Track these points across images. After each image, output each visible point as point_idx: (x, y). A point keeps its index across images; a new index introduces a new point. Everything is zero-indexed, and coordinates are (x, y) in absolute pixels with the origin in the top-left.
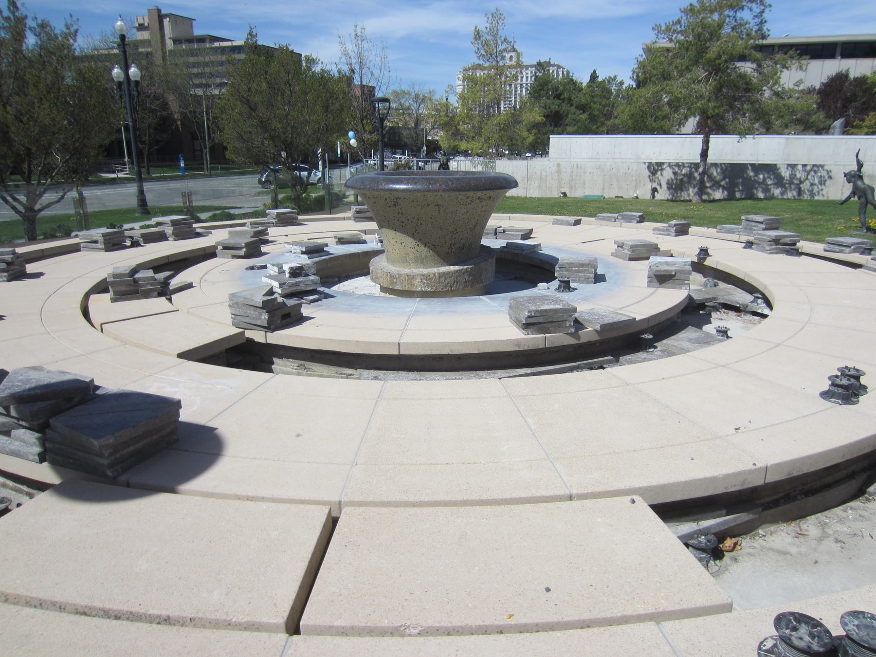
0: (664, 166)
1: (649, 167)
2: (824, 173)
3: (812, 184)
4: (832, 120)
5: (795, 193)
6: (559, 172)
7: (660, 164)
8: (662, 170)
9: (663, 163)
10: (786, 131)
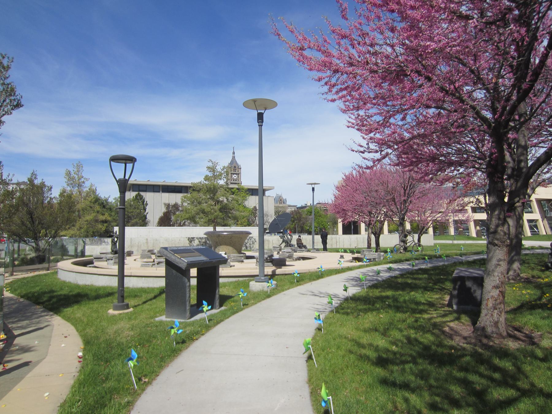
0: (195, 239)
1: (188, 239)
2: (253, 240)
3: (250, 244)
4: (541, 58)
5: (245, 248)
6: (147, 243)
7: (193, 238)
8: (194, 240)
9: (194, 238)
10: (90, 357)
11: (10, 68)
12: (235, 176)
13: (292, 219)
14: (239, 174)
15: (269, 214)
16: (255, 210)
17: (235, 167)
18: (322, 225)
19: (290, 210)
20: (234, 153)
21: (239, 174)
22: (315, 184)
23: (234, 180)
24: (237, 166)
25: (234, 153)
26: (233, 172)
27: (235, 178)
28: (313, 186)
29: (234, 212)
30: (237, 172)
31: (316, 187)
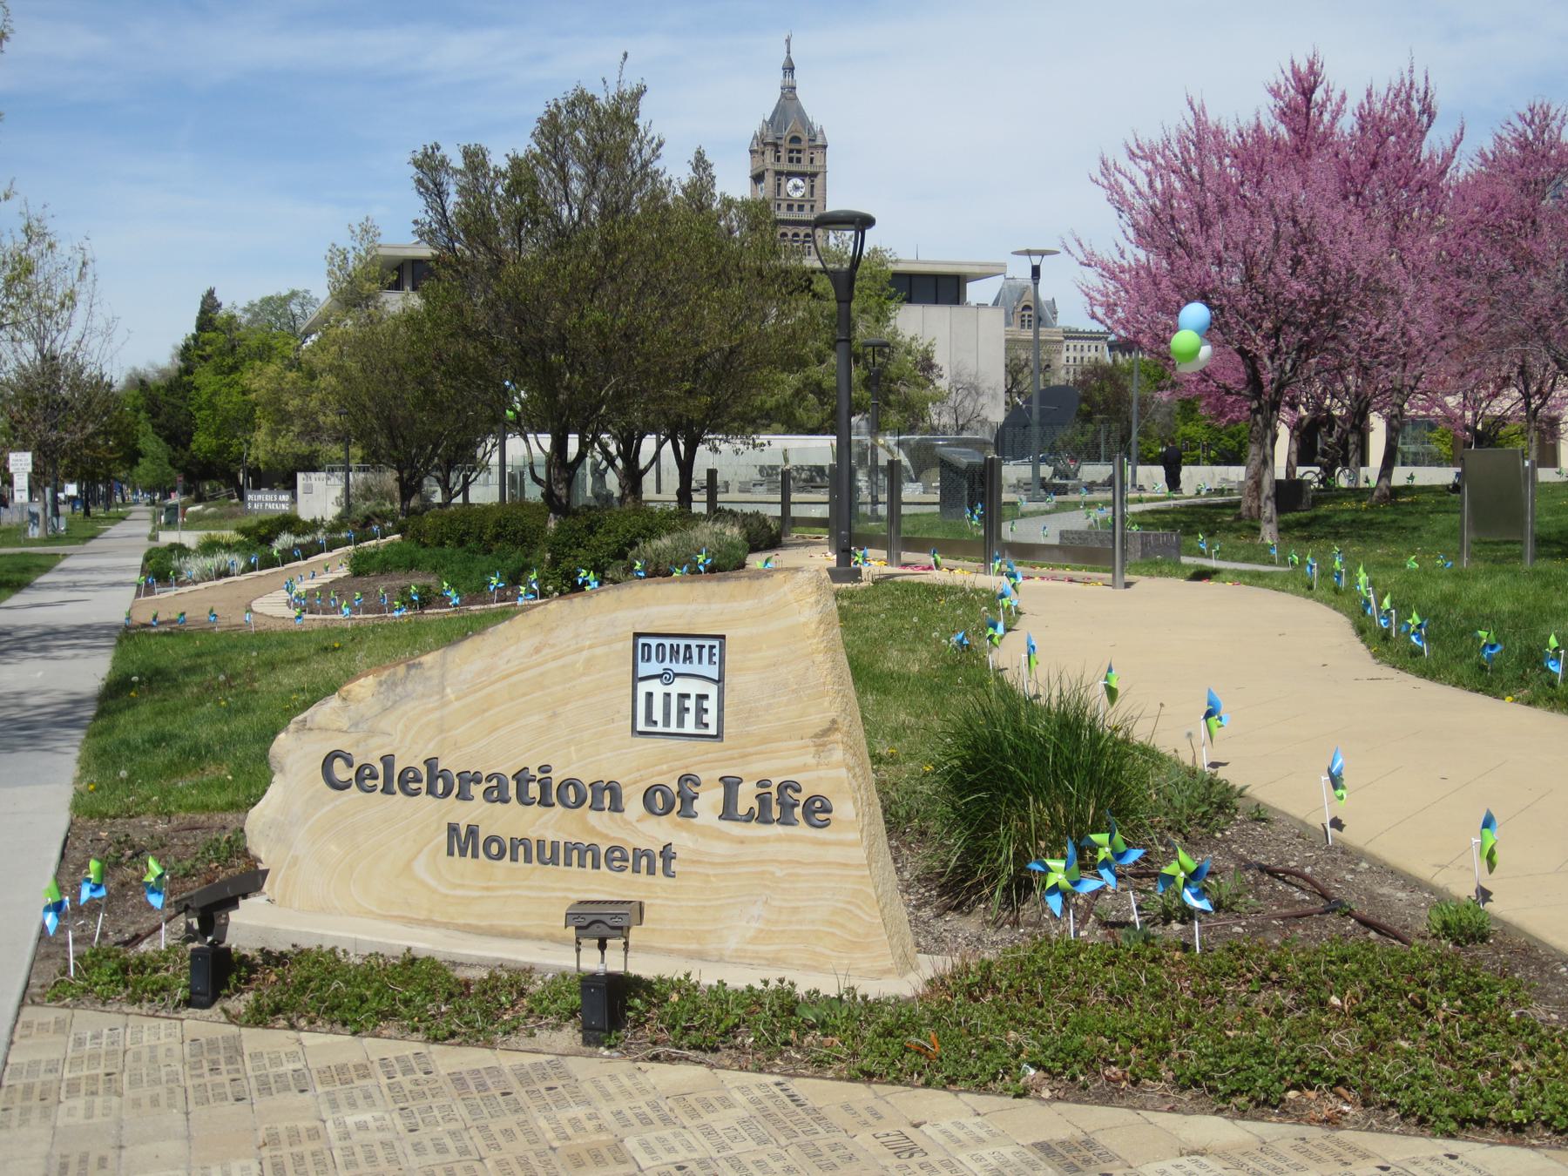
11: (418, 165)
12: (796, 188)
13: (1084, 406)
14: (813, 175)
15: (984, 386)
16: (923, 369)
17: (795, 140)
18: (1232, 436)
19: (1071, 354)
20: (789, 68)
21: (813, 175)
22: (1043, 253)
23: (790, 207)
24: (805, 137)
25: (789, 68)
26: (785, 166)
27: (797, 195)
28: (1036, 260)
29: (903, 389)
30: (805, 167)
31: (1046, 265)
